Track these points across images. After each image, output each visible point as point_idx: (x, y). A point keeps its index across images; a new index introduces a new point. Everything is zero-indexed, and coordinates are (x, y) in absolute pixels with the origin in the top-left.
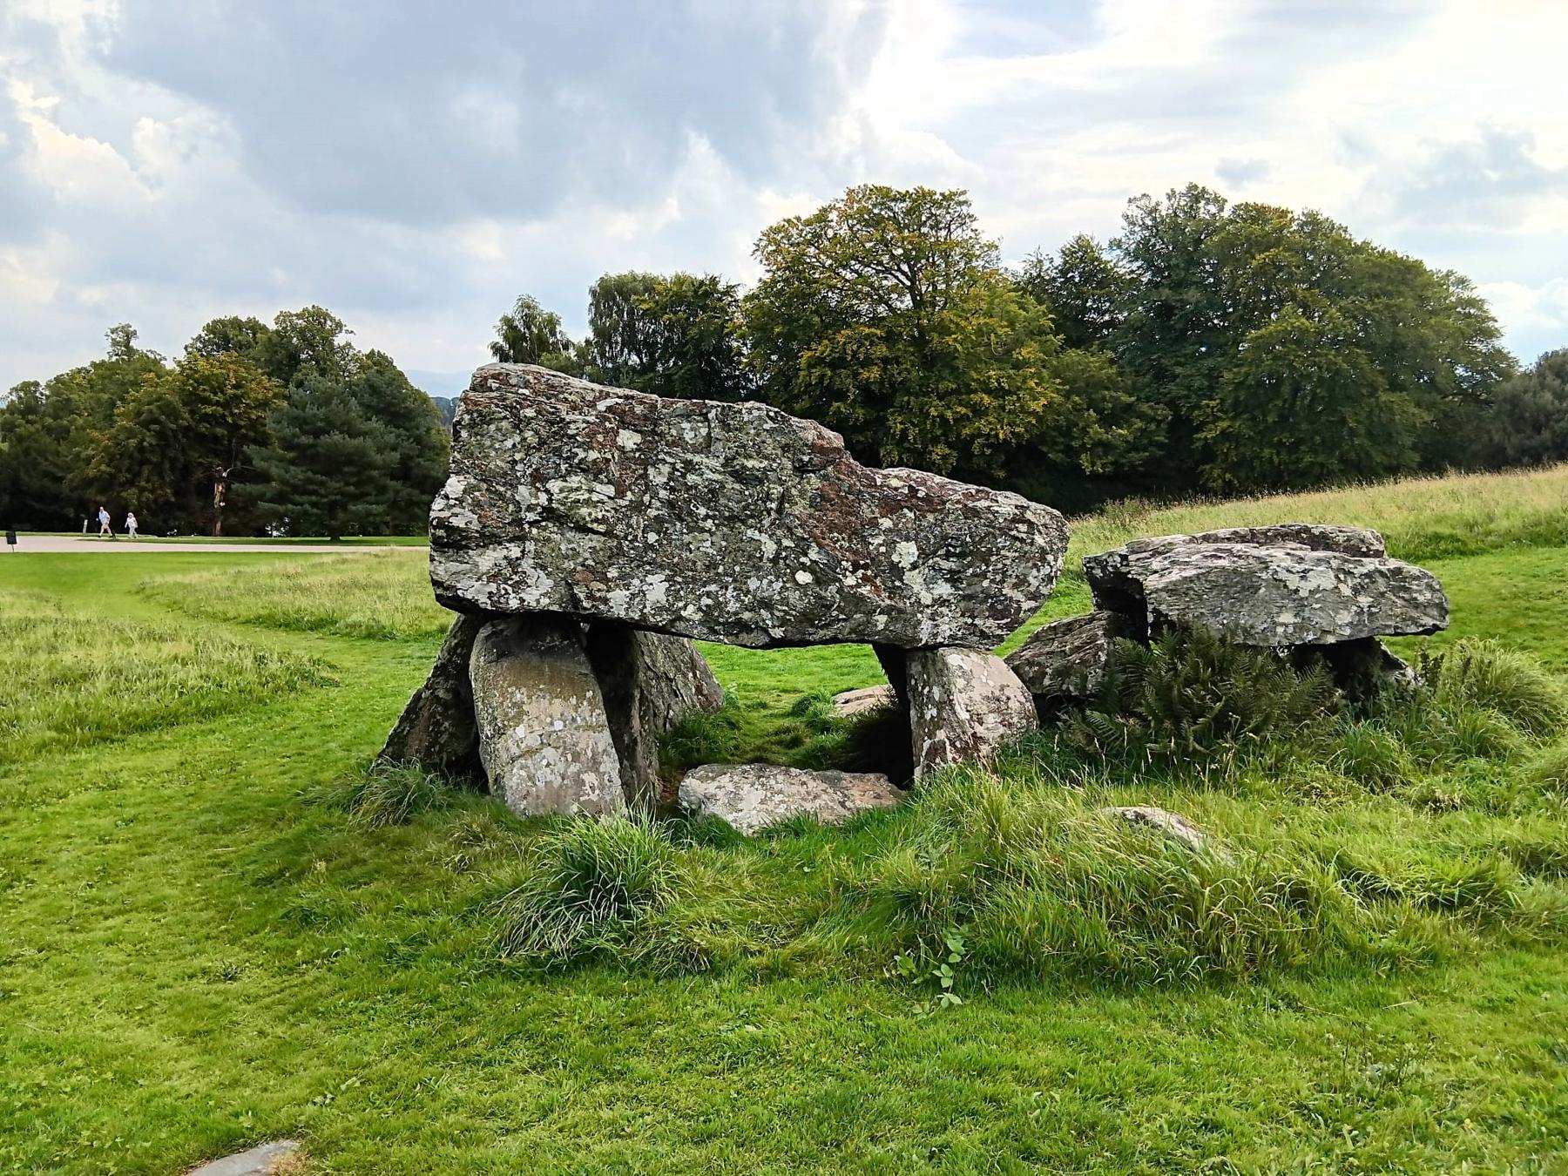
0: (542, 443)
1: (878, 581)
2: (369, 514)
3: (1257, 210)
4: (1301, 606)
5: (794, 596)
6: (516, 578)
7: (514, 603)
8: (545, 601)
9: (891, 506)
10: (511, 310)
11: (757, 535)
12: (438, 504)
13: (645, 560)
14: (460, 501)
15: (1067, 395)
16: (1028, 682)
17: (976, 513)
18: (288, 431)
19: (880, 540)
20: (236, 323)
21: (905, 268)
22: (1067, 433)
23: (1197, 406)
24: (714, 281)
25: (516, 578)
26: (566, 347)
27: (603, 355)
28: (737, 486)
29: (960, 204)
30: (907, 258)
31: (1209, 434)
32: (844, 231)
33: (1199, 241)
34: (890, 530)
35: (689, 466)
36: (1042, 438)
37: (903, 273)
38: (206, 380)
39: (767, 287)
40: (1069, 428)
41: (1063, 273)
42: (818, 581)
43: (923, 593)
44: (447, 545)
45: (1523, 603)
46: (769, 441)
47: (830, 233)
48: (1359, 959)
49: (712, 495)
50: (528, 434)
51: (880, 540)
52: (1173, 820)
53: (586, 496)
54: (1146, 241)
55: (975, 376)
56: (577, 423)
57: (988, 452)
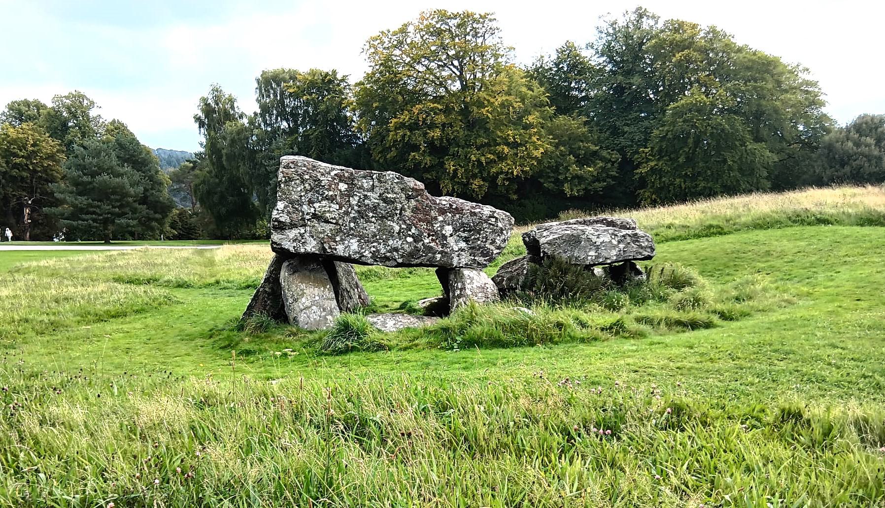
0: (312, 189)
2: (128, 225)
4: (597, 248)
5: (406, 246)
7: (302, 250)
8: (313, 250)
9: (442, 212)
10: (206, 93)
11: (392, 224)
12: (275, 212)
15: (557, 146)
16: (497, 284)
17: (475, 214)
18: (75, 174)
20: (27, 104)
21: (456, 63)
22: (556, 170)
23: (637, 152)
24: (334, 72)
26: (241, 117)
29: (490, 20)
30: (457, 57)
32: (418, 39)
35: (366, 197)
36: (540, 174)
38: (14, 141)
39: (369, 77)
40: (557, 167)
41: (557, 65)
42: (415, 241)
44: (278, 228)
45: (735, 255)
47: (409, 41)
48: (573, 339)
49: (375, 208)
50: (307, 185)
54: (609, 43)
56: (325, 180)
57: (507, 183)
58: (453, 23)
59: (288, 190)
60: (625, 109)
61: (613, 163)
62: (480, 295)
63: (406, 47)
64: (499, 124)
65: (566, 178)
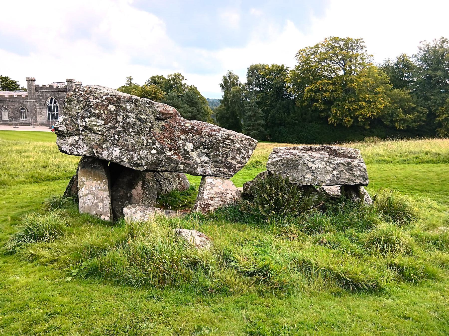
0: (84, 108)
1: (180, 155)
5: (149, 157)
6: (77, 146)
9: (185, 132)
13: (114, 143)
14: (62, 123)
15: (393, 104)
17: (211, 136)
19: (181, 142)
20: (158, 77)
22: (392, 116)
23: (437, 109)
25: (77, 146)
26: (240, 85)
27: (249, 88)
28: (139, 123)
29: (361, 42)
31: (440, 119)
33: (443, 55)
34: (184, 139)
35: (127, 116)
36: (383, 117)
37: (342, 64)
39: (297, 67)
40: (392, 114)
41: (397, 65)
42: (158, 153)
43: (198, 159)
46: (148, 110)
47: (319, 52)
49: (133, 126)
51: (181, 142)
53: (96, 123)
55: (361, 96)
58: (342, 43)
59: (70, 107)
60: (432, 88)
61: (424, 114)
62: (217, 199)
63: (318, 54)
64: (361, 91)
65: (397, 120)
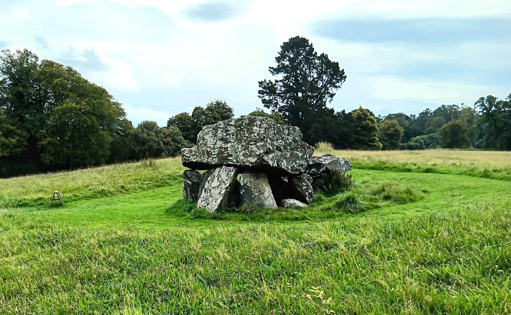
3: (51, 63)
49: (290, 144)
52: (341, 239)
